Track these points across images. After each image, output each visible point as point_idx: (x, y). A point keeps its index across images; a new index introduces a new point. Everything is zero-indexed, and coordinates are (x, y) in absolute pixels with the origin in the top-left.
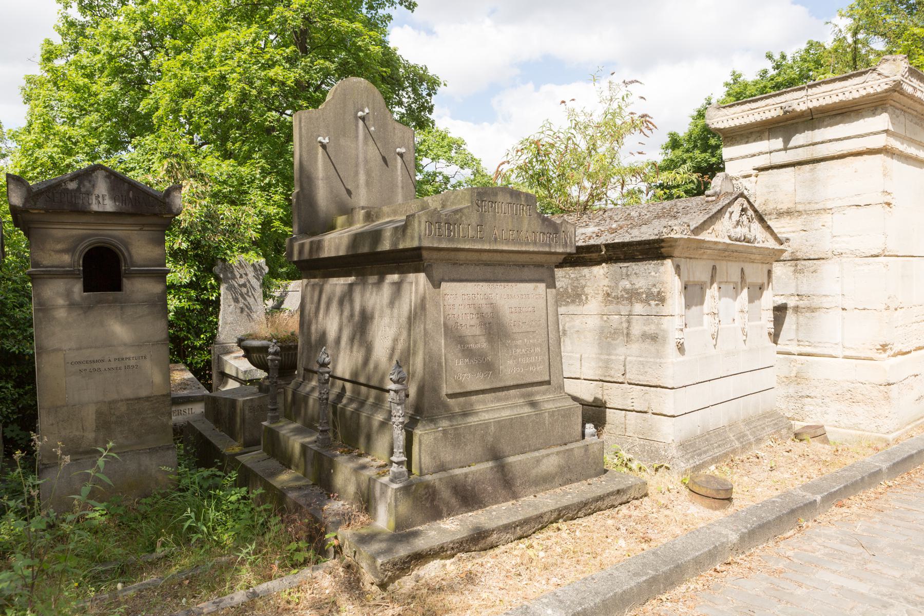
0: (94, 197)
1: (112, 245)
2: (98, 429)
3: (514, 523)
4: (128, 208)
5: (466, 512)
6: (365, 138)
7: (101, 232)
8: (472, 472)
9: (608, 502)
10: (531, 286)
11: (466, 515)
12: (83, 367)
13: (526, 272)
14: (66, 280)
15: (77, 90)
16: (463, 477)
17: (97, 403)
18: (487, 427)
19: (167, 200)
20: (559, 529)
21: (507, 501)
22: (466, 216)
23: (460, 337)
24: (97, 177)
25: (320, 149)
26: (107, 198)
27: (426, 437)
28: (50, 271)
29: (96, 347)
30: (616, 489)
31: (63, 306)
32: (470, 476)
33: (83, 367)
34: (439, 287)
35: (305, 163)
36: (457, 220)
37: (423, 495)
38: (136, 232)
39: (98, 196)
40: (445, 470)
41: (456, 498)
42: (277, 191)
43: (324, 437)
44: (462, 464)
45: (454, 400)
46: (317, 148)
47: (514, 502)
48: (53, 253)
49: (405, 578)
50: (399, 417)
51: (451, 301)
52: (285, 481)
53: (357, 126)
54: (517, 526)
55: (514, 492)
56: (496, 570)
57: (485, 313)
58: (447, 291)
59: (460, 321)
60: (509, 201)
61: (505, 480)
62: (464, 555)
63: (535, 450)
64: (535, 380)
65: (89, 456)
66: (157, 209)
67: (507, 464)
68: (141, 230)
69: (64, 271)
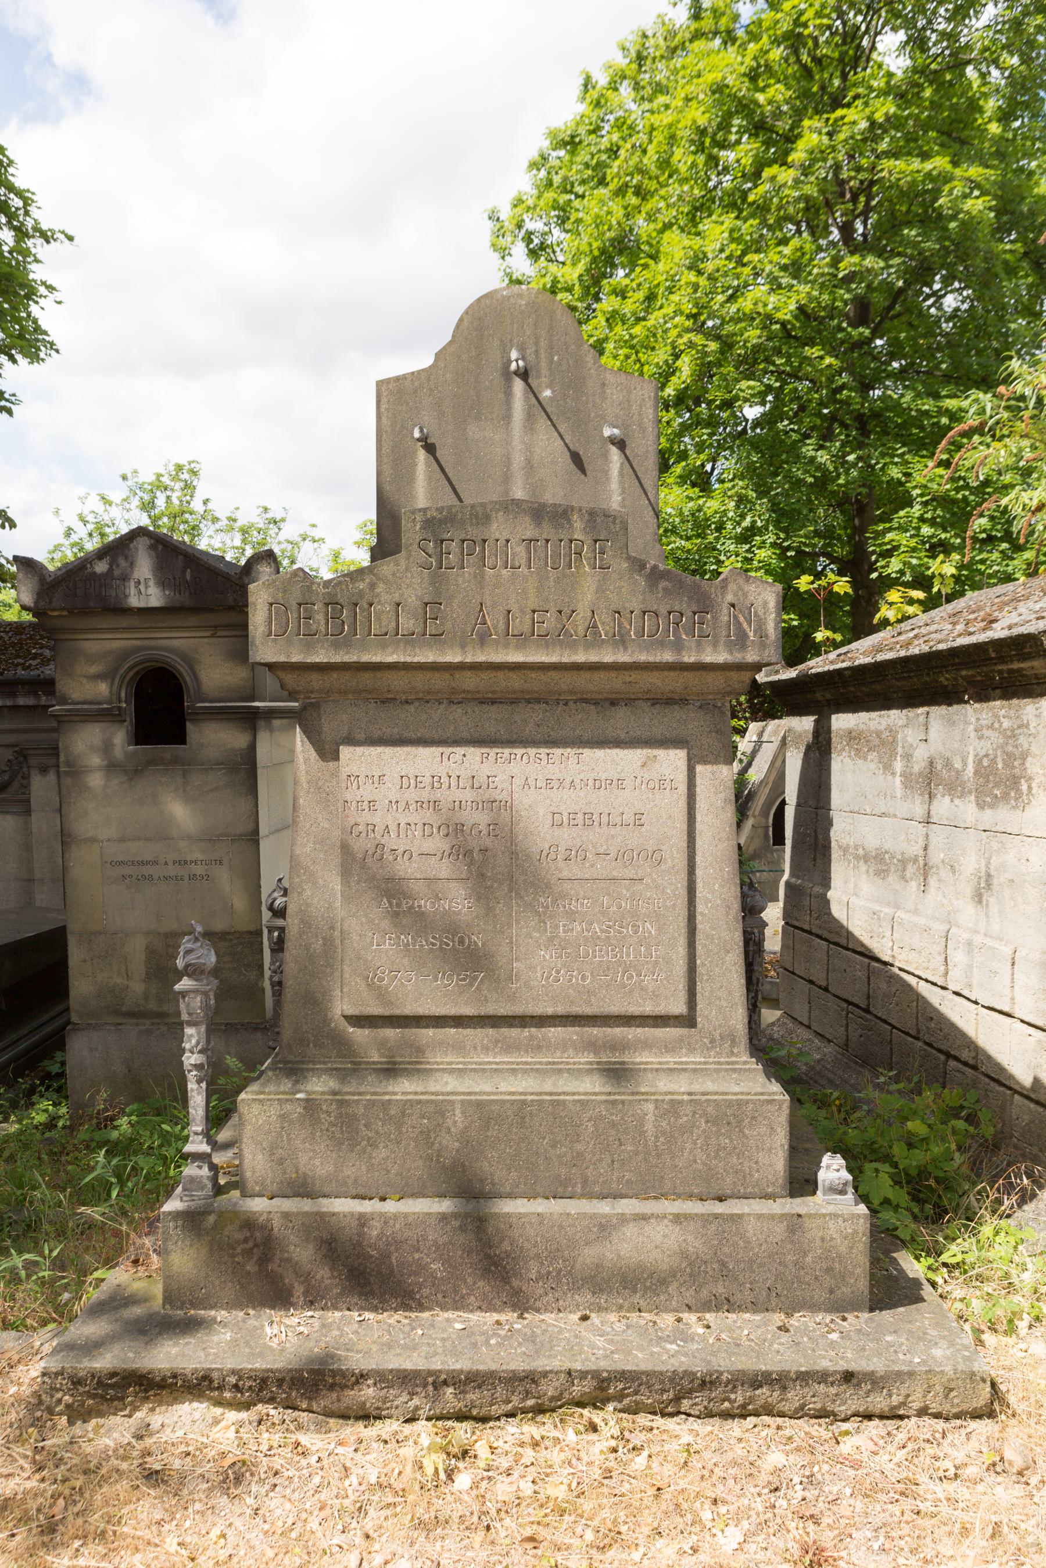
0: (132, 584)
1: (167, 664)
2: (148, 978)
3: (436, 1373)
6: (530, 417)
7: (153, 643)
9: (794, 1397)
10: (629, 759)
12: (128, 870)
13: (621, 719)
14: (103, 725)
16: (354, 1223)
17: (148, 933)
18: (442, 1113)
20: (593, 1428)
21: (491, 1308)
22: (386, 582)
23: (390, 879)
24: (137, 549)
25: (422, 455)
26: (151, 583)
28: (78, 710)
30: (843, 1366)
32: (377, 1224)
33: (128, 870)
34: (336, 757)
36: (361, 594)
37: (238, 1243)
38: (206, 640)
39: (139, 582)
41: (332, 1269)
42: (764, 542)
44: (362, 1191)
45: (367, 1031)
46: (415, 453)
47: (508, 1316)
48: (85, 681)
49: (115, 1420)
50: (192, 1052)
51: (367, 792)
53: (508, 394)
55: (517, 1293)
57: (468, 824)
58: (354, 769)
59: (391, 841)
60: (528, 535)
61: (487, 1256)
63: (604, 1197)
64: (615, 1009)
67: (498, 1215)
68: (212, 636)
69: (98, 710)
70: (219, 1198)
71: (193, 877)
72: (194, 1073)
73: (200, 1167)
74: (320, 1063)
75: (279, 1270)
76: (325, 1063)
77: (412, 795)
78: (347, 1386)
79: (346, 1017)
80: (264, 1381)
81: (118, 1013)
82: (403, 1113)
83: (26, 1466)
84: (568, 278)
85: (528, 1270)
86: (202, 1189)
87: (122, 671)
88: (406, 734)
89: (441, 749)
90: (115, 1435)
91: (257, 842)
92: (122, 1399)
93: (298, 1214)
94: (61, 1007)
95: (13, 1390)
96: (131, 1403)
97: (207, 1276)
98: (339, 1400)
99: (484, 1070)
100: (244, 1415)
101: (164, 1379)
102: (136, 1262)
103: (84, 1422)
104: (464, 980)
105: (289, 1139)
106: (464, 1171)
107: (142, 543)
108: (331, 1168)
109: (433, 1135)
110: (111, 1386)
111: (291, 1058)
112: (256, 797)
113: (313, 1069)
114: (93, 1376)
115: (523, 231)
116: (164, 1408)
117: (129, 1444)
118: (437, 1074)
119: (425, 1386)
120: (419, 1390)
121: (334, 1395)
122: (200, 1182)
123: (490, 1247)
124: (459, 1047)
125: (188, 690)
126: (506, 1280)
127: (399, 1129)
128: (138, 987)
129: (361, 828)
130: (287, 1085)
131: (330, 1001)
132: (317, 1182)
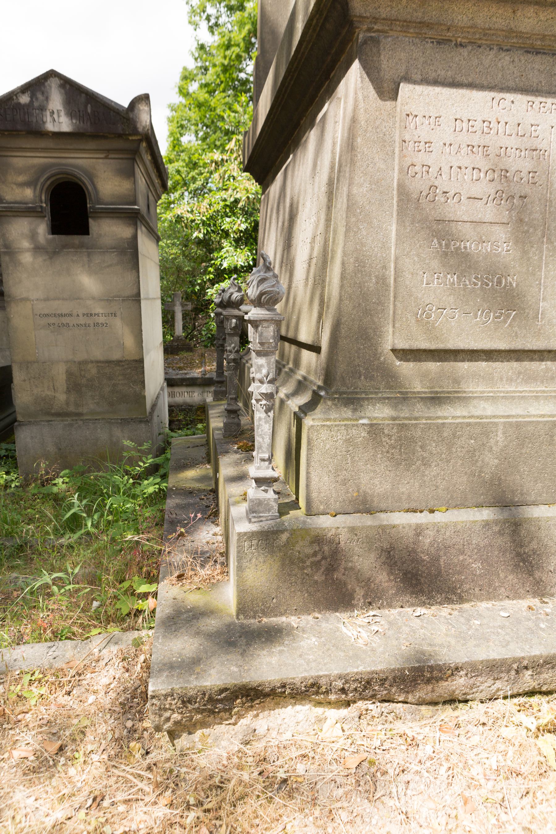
2: (68, 391)
3: (519, 660)
4: (87, 127)
5: (412, 605)
7: (63, 161)
8: (434, 525)
11: (409, 610)
12: (52, 320)
15: (200, 105)
16: (411, 533)
17: (67, 362)
19: (131, 116)
21: (517, 596)
24: (51, 87)
26: (62, 113)
27: (324, 434)
28: (11, 207)
29: (63, 299)
31: (28, 250)
32: (430, 533)
33: (52, 320)
35: (269, 8)
38: (101, 161)
39: (53, 113)
40: (369, 511)
41: (390, 573)
43: (230, 421)
44: (413, 505)
45: (411, 364)
47: (535, 602)
48: (14, 187)
49: (220, 729)
50: (261, 382)
51: (424, 133)
52: (187, 480)
54: (526, 668)
55: (538, 582)
56: (443, 770)
57: (513, 169)
58: (413, 108)
59: (443, 184)
62: (375, 708)
65: (61, 418)
66: (120, 128)
67: (529, 520)
68: (106, 158)
69: (26, 208)
70: (284, 518)
71: (96, 325)
72: (264, 402)
73: (266, 491)
74: (372, 393)
75: (344, 578)
76: (376, 393)
77: (464, 138)
78: (442, 679)
79: (394, 351)
80: (368, 682)
81: (48, 414)
82: (454, 435)
83: (147, 789)
84: (236, 38)
85: (549, 563)
86: (269, 511)
87: (42, 180)
88: (459, 78)
89: (492, 94)
90: (224, 743)
91: (139, 301)
92: (230, 710)
93: (363, 528)
94: (10, 411)
95: (91, 698)
96: (237, 713)
97: (279, 587)
98: (433, 691)
99: (513, 398)
100: (344, 712)
101: (273, 690)
102: (180, 577)
103: (190, 733)
104: (499, 317)
105: (353, 462)
106: (500, 484)
107: (54, 83)
108: (388, 486)
109: (477, 454)
110: (219, 701)
111: (344, 389)
112: (138, 271)
113: (368, 399)
114: (204, 694)
115: (206, 14)
116: (266, 713)
117: (239, 751)
118: (475, 402)
119: (509, 671)
120: (502, 675)
121: (430, 687)
122: (268, 504)
123: (522, 546)
124: (489, 379)
125: (90, 196)
126: (530, 573)
127: (449, 448)
128: (62, 397)
129: (417, 168)
130: (347, 413)
131: (380, 336)
132: (376, 499)
